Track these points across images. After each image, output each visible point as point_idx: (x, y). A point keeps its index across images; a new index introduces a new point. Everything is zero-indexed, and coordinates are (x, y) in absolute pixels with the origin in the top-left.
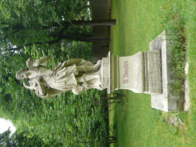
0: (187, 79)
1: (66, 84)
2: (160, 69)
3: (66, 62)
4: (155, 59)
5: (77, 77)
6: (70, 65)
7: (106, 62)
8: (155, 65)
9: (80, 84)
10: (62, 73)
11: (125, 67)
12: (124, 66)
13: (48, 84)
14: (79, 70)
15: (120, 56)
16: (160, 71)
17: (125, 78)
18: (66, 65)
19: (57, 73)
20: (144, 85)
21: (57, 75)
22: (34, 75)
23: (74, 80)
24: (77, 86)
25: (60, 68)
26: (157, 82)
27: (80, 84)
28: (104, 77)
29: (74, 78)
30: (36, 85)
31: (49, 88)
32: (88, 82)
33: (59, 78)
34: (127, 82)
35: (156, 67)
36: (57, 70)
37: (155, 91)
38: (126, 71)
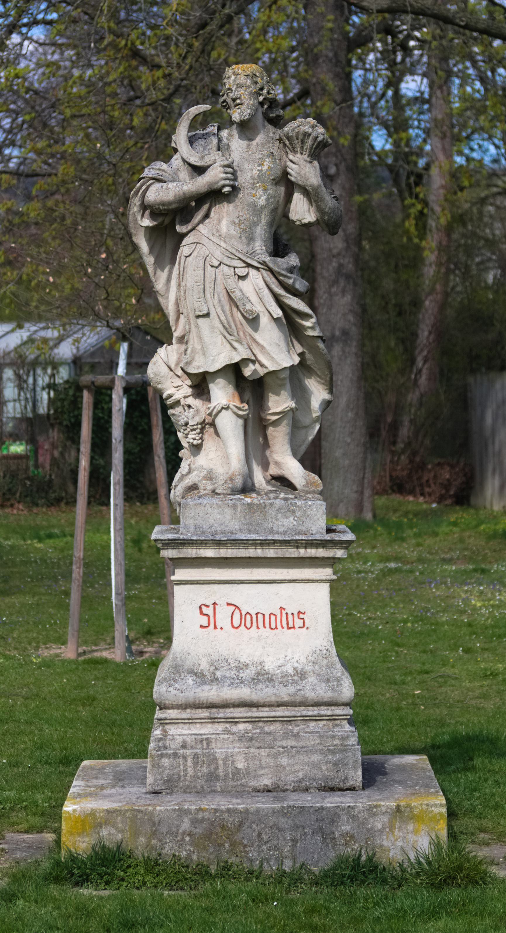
3: (306, 316)
5: (234, 372)
9: (201, 385)
11: (278, 613)
13: (201, 227)
15: (335, 587)
19: (253, 272)
20: (237, 703)
22: (248, 157)
23: (217, 354)
24: (189, 375)
25: (280, 291)
27: (201, 385)
30: (199, 170)
31: (180, 229)
32: (209, 424)
34: (204, 621)
36: (271, 270)
38: (260, 617)
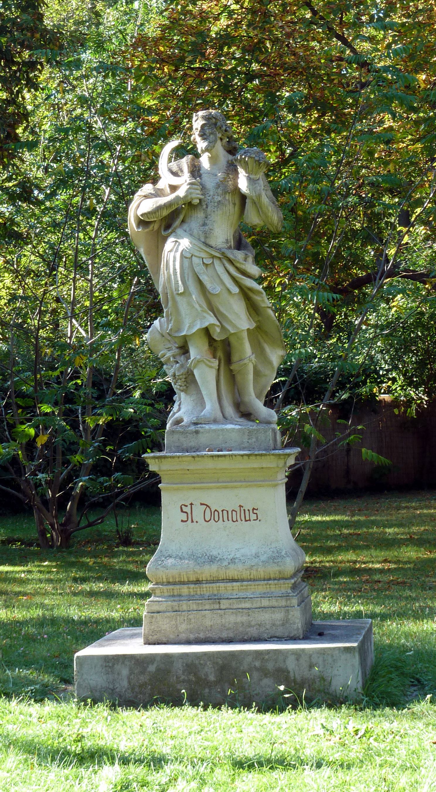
0: (265, 780)
1: (178, 294)
2: (231, 635)
3: (258, 293)
4: (266, 617)
6: (253, 308)
7: (254, 440)
8: (245, 619)
10: (220, 280)
11: (238, 510)
12: (240, 506)
14: (233, 340)
16: (224, 635)
17: (198, 512)
18: (251, 294)
21: (209, 261)
26: (183, 627)
28: (200, 435)
29: (198, 326)
30: (174, 188)
33: (199, 269)
34: (184, 517)
35: (239, 619)
37: (152, 617)
38: (225, 512)
